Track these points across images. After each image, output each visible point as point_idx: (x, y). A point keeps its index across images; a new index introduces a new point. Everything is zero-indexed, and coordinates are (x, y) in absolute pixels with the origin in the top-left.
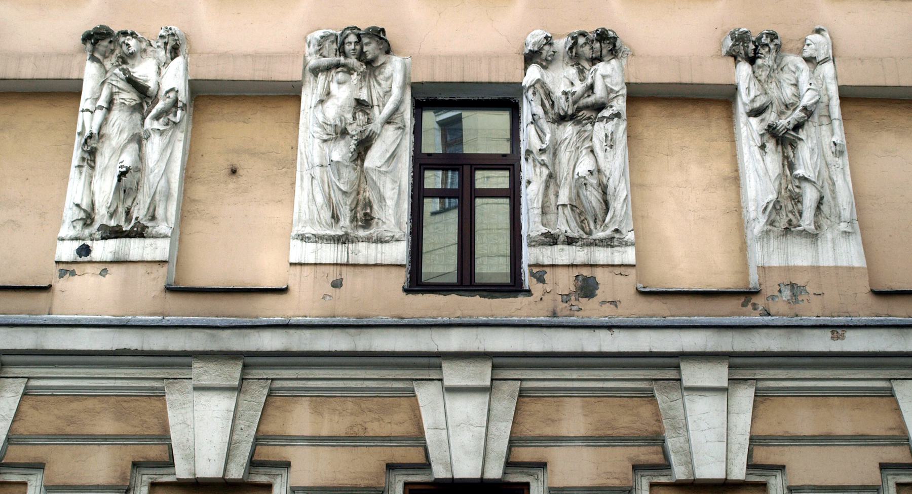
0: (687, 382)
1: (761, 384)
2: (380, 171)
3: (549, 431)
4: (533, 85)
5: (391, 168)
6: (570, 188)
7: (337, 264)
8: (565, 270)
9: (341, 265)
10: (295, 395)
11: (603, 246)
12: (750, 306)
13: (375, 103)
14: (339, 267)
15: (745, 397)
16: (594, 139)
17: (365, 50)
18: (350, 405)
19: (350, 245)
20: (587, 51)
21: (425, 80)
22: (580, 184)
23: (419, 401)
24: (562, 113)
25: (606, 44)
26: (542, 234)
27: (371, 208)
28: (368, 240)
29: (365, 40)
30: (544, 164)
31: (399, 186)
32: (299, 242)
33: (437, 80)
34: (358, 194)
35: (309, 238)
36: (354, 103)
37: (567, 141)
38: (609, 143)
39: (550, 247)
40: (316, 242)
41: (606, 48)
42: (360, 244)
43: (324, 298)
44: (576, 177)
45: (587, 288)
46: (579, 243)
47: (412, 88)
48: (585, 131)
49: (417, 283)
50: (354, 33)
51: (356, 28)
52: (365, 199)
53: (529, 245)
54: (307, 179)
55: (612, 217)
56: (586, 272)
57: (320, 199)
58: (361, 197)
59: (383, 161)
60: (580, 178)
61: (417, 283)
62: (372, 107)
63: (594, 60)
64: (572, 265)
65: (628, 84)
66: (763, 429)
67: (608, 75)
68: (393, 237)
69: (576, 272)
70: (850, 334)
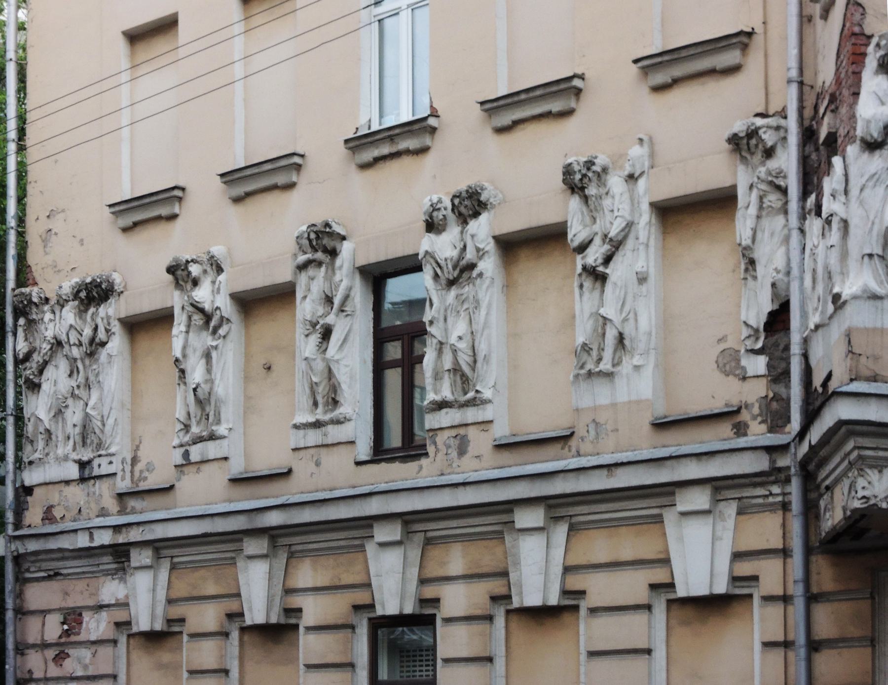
0: (518, 525)
1: (574, 520)
3: (441, 573)
10: (305, 554)
12: (567, 449)
15: (561, 532)
18: (331, 561)
23: (861, 325)
25: (470, 204)
39: (438, 412)
66: (573, 561)
67: (482, 229)
70: (620, 471)
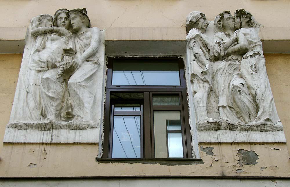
2: (80, 85)
4: (194, 38)
5: (88, 85)
6: (227, 97)
7: (42, 143)
8: (229, 147)
9: (46, 144)
11: (258, 131)
13: (78, 50)
14: (44, 146)
16: (242, 69)
17: (72, 23)
19: (54, 131)
20: (230, 23)
21: (115, 39)
22: (236, 91)
24: (216, 55)
26: (208, 122)
27: (72, 109)
28: (69, 127)
29: (72, 16)
30: (207, 81)
31: (95, 96)
32: (13, 130)
33: (124, 39)
34: (63, 102)
35: (21, 126)
36: (62, 52)
37: (222, 70)
38: (254, 70)
40: (27, 129)
41: (244, 20)
42: (62, 131)
43: (29, 166)
44: (231, 87)
45: (249, 158)
46: (239, 128)
47: (106, 46)
48: (235, 64)
49: (106, 157)
50: (64, 12)
51: (65, 9)
52: (67, 105)
53: (199, 130)
54: (23, 94)
55: (263, 113)
56: (246, 148)
57: (32, 104)
58: (64, 104)
59: (83, 79)
60: (234, 87)
61: (106, 157)
62: (76, 53)
63: (235, 29)
64: (235, 143)
65: (263, 41)
68: (89, 125)
69: (239, 147)
